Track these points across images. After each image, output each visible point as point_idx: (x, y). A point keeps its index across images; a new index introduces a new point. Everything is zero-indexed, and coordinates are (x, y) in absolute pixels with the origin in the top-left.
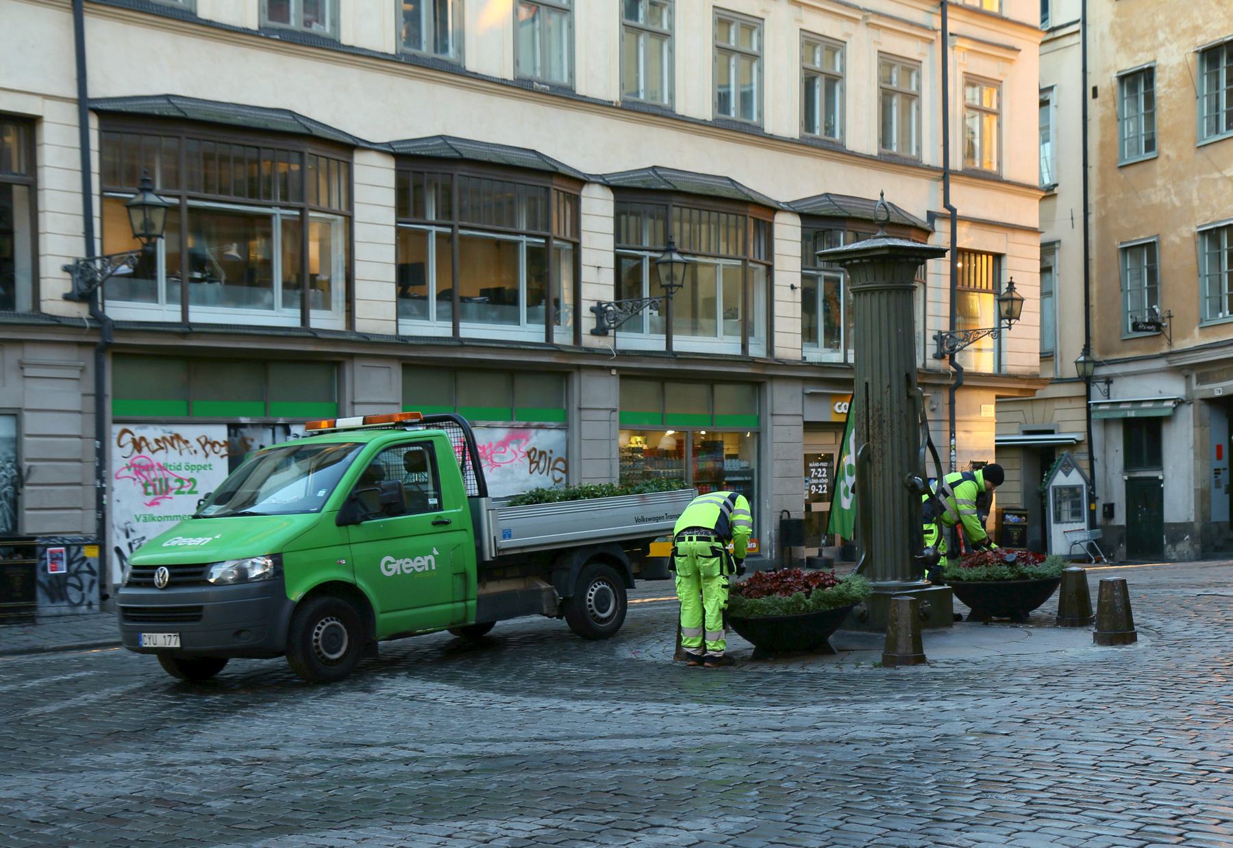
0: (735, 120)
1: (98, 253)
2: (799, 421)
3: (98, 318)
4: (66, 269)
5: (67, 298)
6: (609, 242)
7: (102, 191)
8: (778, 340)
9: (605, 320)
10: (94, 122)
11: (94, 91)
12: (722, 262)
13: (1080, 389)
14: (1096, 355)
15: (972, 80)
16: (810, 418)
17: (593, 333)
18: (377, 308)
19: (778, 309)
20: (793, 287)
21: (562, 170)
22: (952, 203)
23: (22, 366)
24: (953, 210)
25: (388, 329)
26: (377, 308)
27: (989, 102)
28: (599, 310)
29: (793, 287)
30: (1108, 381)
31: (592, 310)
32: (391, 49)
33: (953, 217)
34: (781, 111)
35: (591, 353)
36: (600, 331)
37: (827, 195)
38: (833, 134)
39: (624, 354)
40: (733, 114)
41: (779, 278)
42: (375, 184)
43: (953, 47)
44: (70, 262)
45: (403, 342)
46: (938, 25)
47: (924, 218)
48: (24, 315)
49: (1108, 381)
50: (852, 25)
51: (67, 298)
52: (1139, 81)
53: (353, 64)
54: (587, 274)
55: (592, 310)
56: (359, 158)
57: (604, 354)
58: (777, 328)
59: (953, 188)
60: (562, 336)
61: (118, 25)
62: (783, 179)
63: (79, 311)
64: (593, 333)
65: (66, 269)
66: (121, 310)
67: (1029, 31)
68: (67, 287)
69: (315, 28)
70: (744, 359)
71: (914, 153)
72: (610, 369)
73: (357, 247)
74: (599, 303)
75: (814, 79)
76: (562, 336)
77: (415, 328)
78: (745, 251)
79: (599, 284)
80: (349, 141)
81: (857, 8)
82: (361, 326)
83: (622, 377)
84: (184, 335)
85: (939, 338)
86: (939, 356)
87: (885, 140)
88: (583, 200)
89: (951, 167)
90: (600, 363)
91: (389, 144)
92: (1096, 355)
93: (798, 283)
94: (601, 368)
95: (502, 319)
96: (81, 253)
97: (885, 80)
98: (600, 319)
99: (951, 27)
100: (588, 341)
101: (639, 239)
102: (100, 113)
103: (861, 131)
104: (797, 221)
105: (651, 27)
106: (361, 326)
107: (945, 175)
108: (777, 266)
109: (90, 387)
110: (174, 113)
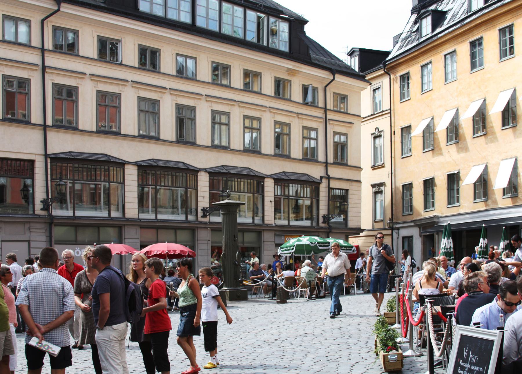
0: (253, 150)
1: (50, 197)
2: (273, 243)
3: (50, 215)
4: (41, 202)
5: (41, 209)
6: (207, 189)
7: (51, 179)
8: (266, 218)
9: (206, 212)
10: (49, 161)
11: (49, 152)
12: (180, 189)
13: (390, 232)
14: (394, 221)
15: (335, 133)
16: (277, 242)
17: (202, 217)
18: (269, 218)
19: (266, 208)
20: (271, 202)
21: (160, 164)
22: (329, 173)
23: (29, 229)
24: (329, 176)
25: (136, 216)
26: (132, 210)
27: (255, 124)
28: (204, 210)
29: (271, 202)
30: (398, 229)
31: (202, 210)
32: (301, 158)
33: (328, 178)
34: (268, 146)
35: (201, 223)
36: (204, 216)
37: (284, 172)
38: (314, 157)
39: (211, 223)
40: (339, 161)
41: (266, 199)
42: (131, 175)
43: (330, 124)
44: (42, 200)
45: (140, 220)
46: (40, 63)
47: (319, 178)
48: (30, 215)
49: (398, 229)
50: (293, 118)
51: (41, 209)
52: (407, 130)
53: (263, 158)
54: (200, 199)
55: (202, 210)
56: (127, 167)
57: (205, 223)
58: (265, 214)
59: (329, 168)
60: (314, 224)
61: (56, 133)
62: (202, 160)
63: (43, 213)
64: (202, 217)
65: (41, 202)
66: (57, 212)
67: (166, 76)
68: (42, 207)
69: (343, 162)
70: (253, 224)
71: (258, 149)
72: (208, 228)
73: (126, 193)
74: (204, 208)
75: (337, 145)
76: (191, 218)
77: (143, 216)
78: (74, 177)
79: (204, 202)
80: (262, 175)
81: (295, 113)
82: (127, 216)
83: (212, 230)
84: (74, 220)
85: (324, 217)
86: (324, 222)
87: (213, 141)
88: (320, 188)
89: (329, 161)
90: (205, 226)
91: (136, 162)
92: (394, 221)
93: (273, 200)
94: (204, 228)
95: (96, 209)
96: (46, 198)
97: (213, 118)
98: (324, 219)
99: (329, 117)
100: (200, 219)
101: (219, 188)
102: (51, 158)
103: (296, 152)
104: (273, 181)
105: (111, 105)
106: (127, 216)
107: (326, 164)
108: (265, 194)
109: (48, 234)
110: (287, 178)
